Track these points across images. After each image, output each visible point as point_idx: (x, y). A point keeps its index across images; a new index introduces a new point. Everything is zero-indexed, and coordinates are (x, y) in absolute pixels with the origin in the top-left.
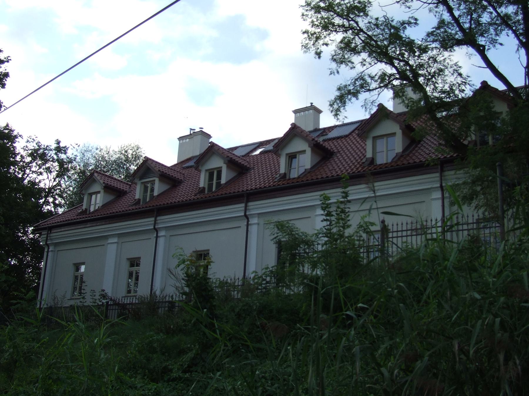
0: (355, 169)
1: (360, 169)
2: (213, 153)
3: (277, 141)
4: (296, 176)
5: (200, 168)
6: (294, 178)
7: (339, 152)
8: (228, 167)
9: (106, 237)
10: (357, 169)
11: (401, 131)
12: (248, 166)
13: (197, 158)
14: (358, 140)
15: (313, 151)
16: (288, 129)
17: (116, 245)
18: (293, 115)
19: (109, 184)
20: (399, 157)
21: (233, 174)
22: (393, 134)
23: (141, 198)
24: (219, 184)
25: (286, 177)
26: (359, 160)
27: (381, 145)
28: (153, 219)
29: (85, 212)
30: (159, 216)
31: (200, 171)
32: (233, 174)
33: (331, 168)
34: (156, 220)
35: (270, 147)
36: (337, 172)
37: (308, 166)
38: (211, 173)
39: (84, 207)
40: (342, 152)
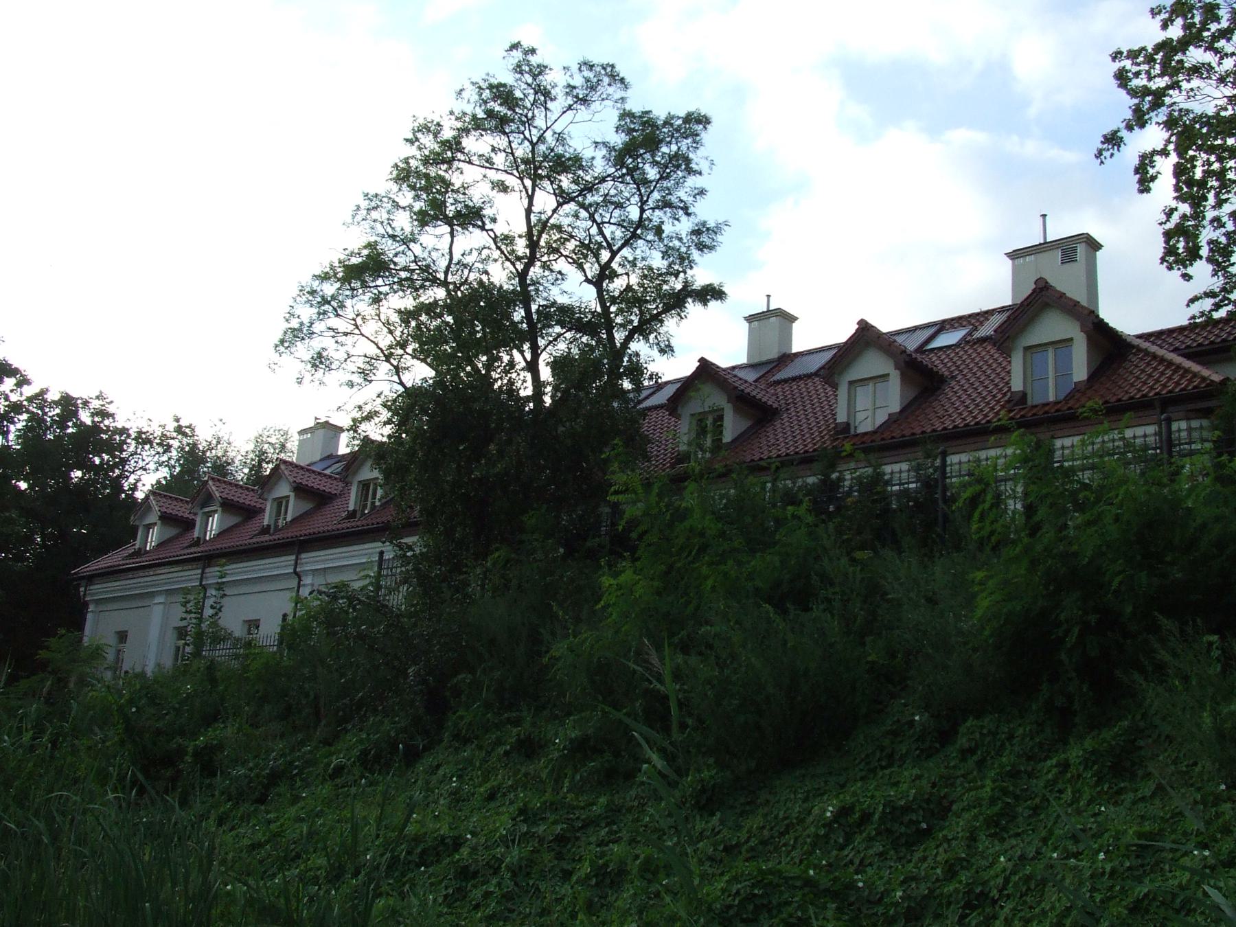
0: (991, 415)
1: (1002, 413)
2: (1046, 306)
3: (996, 321)
4: (869, 429)
5: (265, 496)
6: (865, 434)
7: (955, 377)
8: (296, 496)
9: (152, 595)
10: (986, 416)
11: (898, 372)
12: (775, 405)
13: (678, 385)
14: (996, 355)
15: (904, 378)
16: (1030, 292)
17: (161, 607)
18: (1009, 263)
19: (230, 497)
20: (893, 420)
21: (744, 425)
22: (885, 377)
23: (272, 523)
24: (718, 445)
25: (1025, 403)
26: (999, 396)
27: (863, 398)
28: (293, 557)
29: (197, 542)
30: (209, 566)
31: (835, 387)
32: (744, 425)
33: (941, 413)
34: (203, 573)
35: (987, 330)
36: (964, 419)
37: (895, 407)
38: (700, 419)
39: (196, 535)
40: (959, 377)
